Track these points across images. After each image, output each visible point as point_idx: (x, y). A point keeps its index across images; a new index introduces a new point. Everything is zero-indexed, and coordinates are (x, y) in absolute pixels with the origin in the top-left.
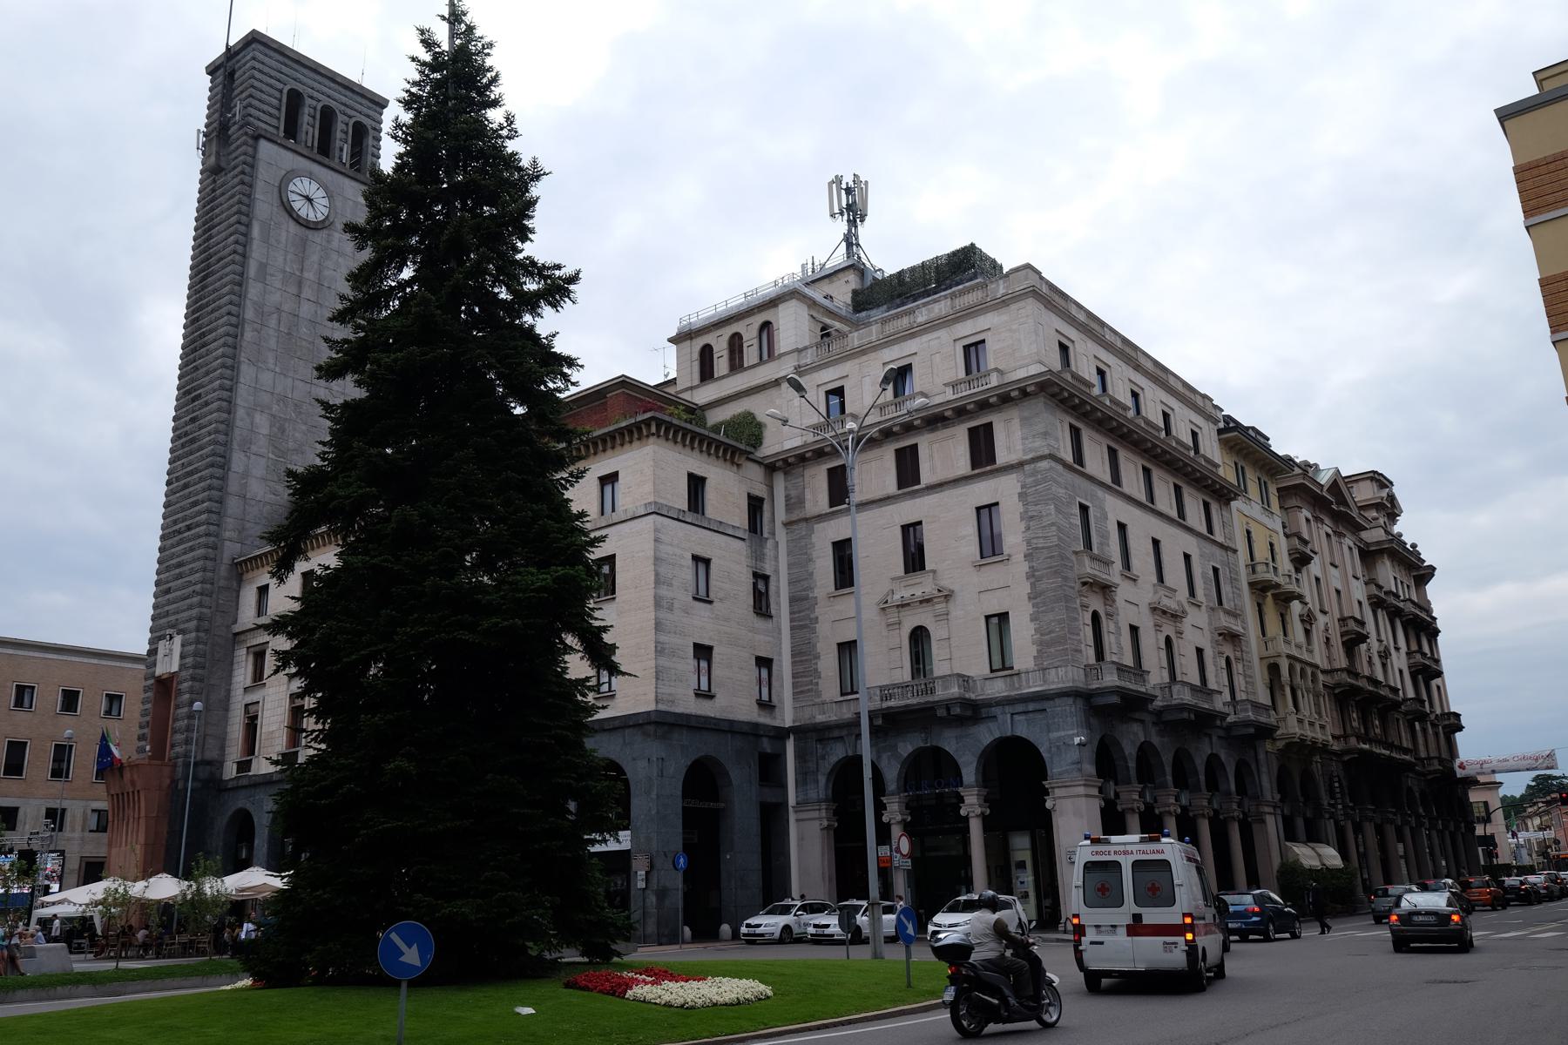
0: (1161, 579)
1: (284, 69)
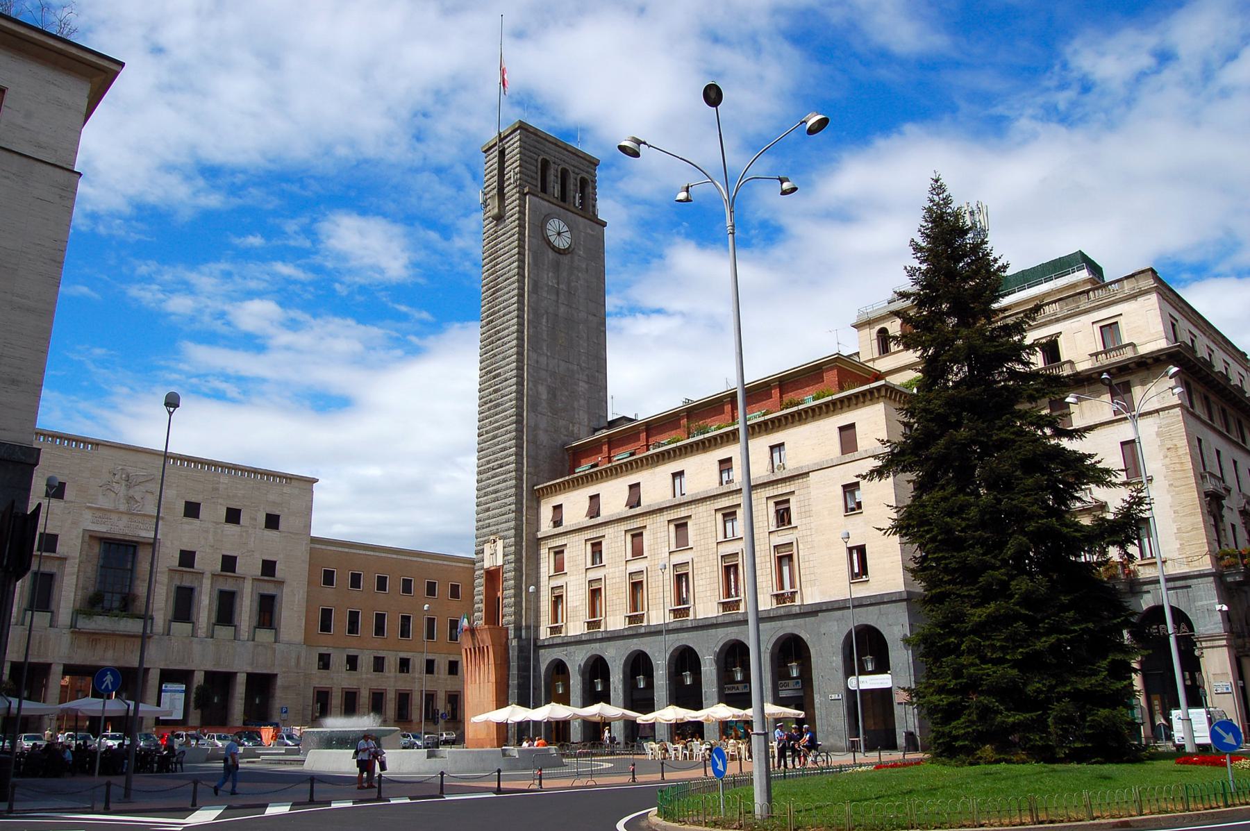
0: (1240, 491)
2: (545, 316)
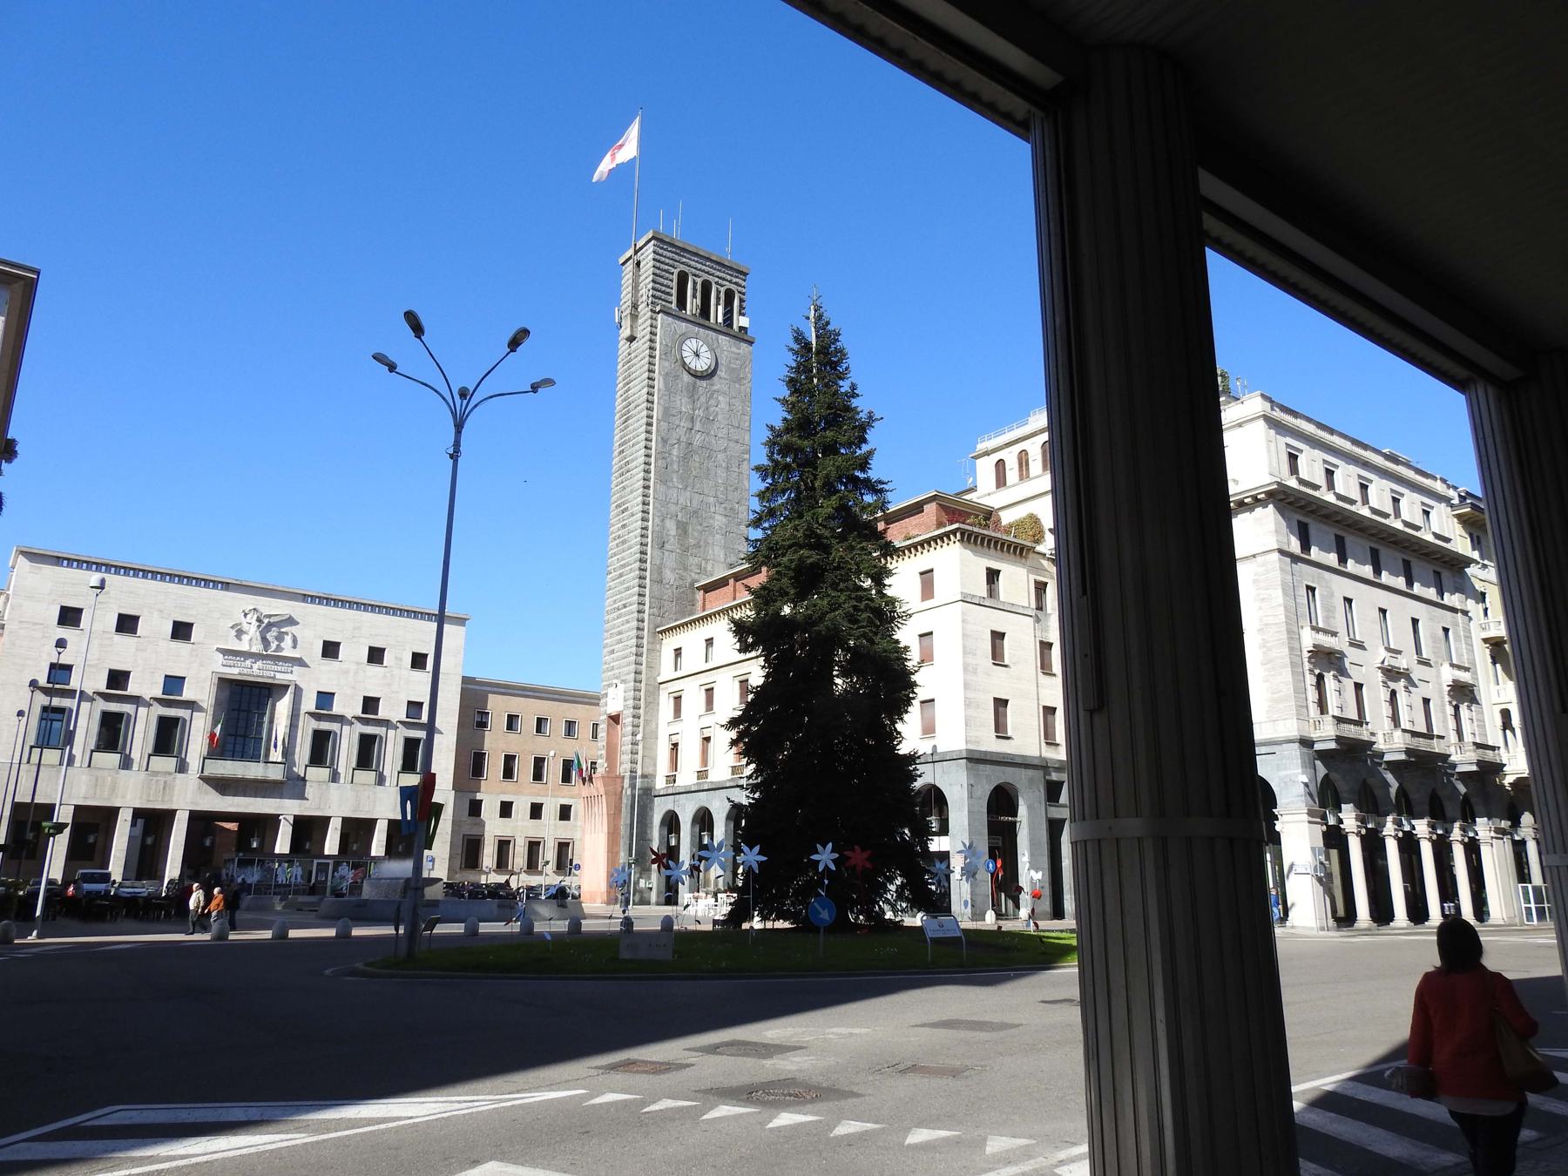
1: (676, 257)
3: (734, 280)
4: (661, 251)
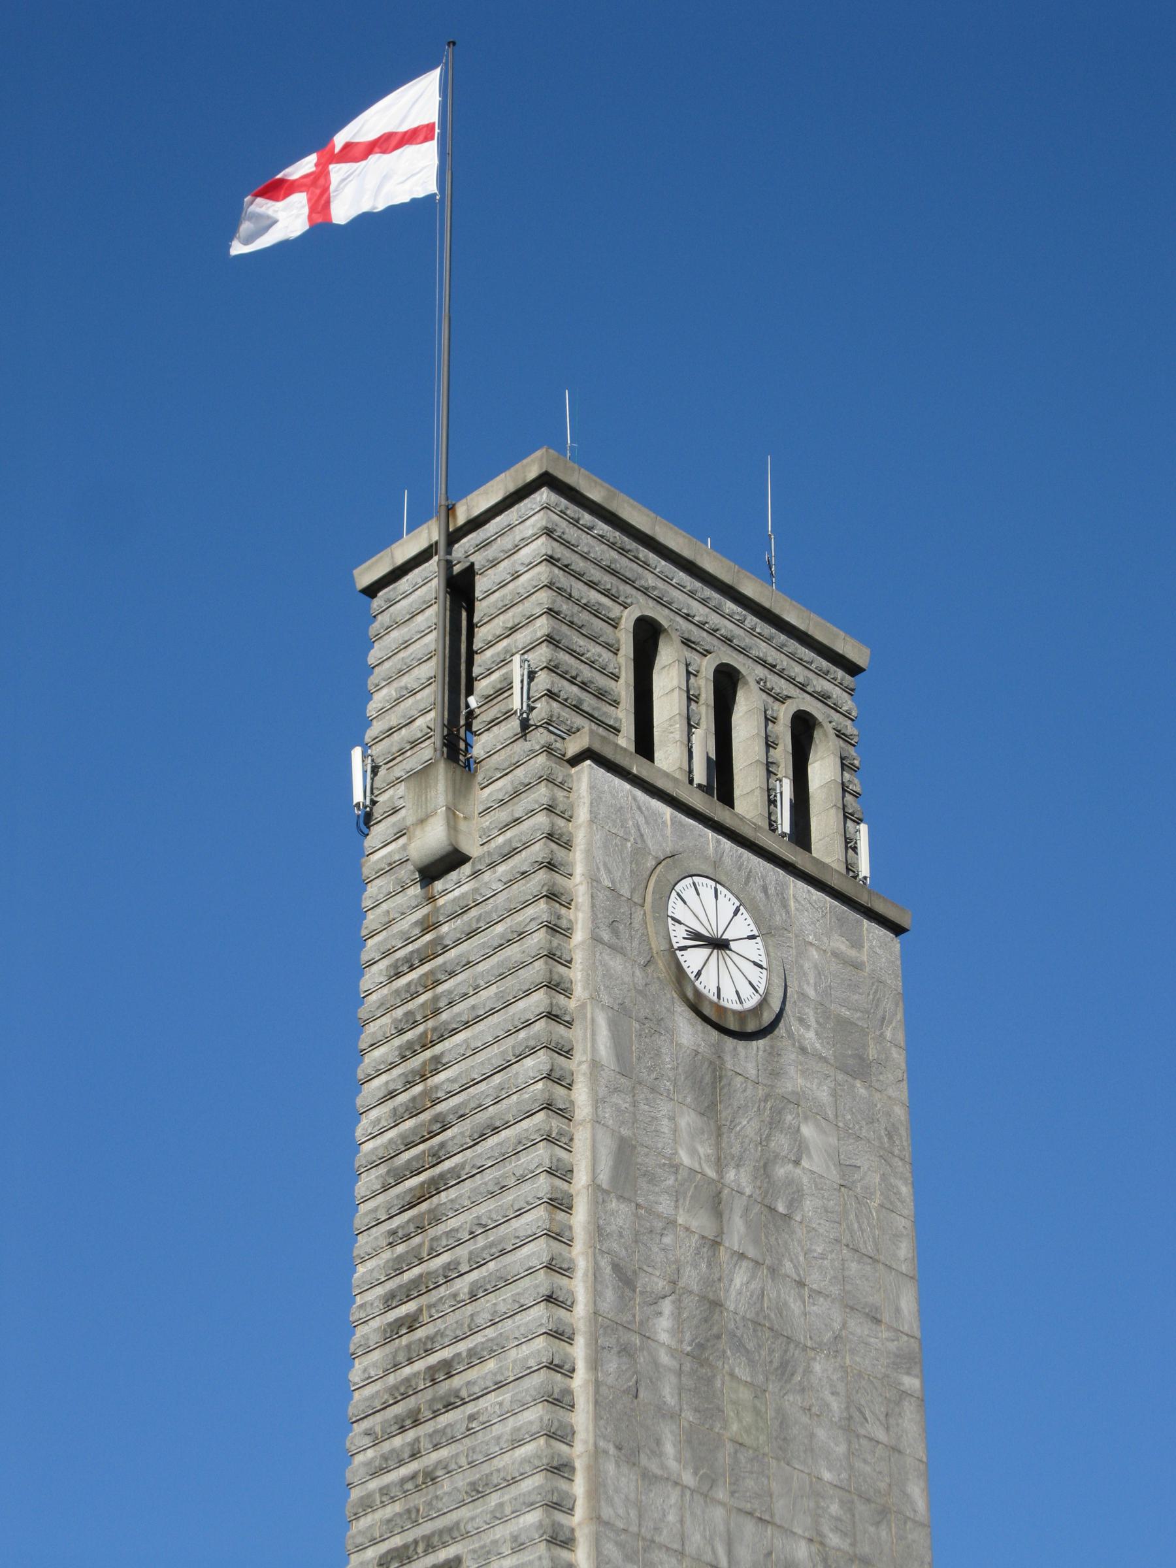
1: (623, 564)
2: (667, 1306)
3: (821, 685)
4: (572, 534)
